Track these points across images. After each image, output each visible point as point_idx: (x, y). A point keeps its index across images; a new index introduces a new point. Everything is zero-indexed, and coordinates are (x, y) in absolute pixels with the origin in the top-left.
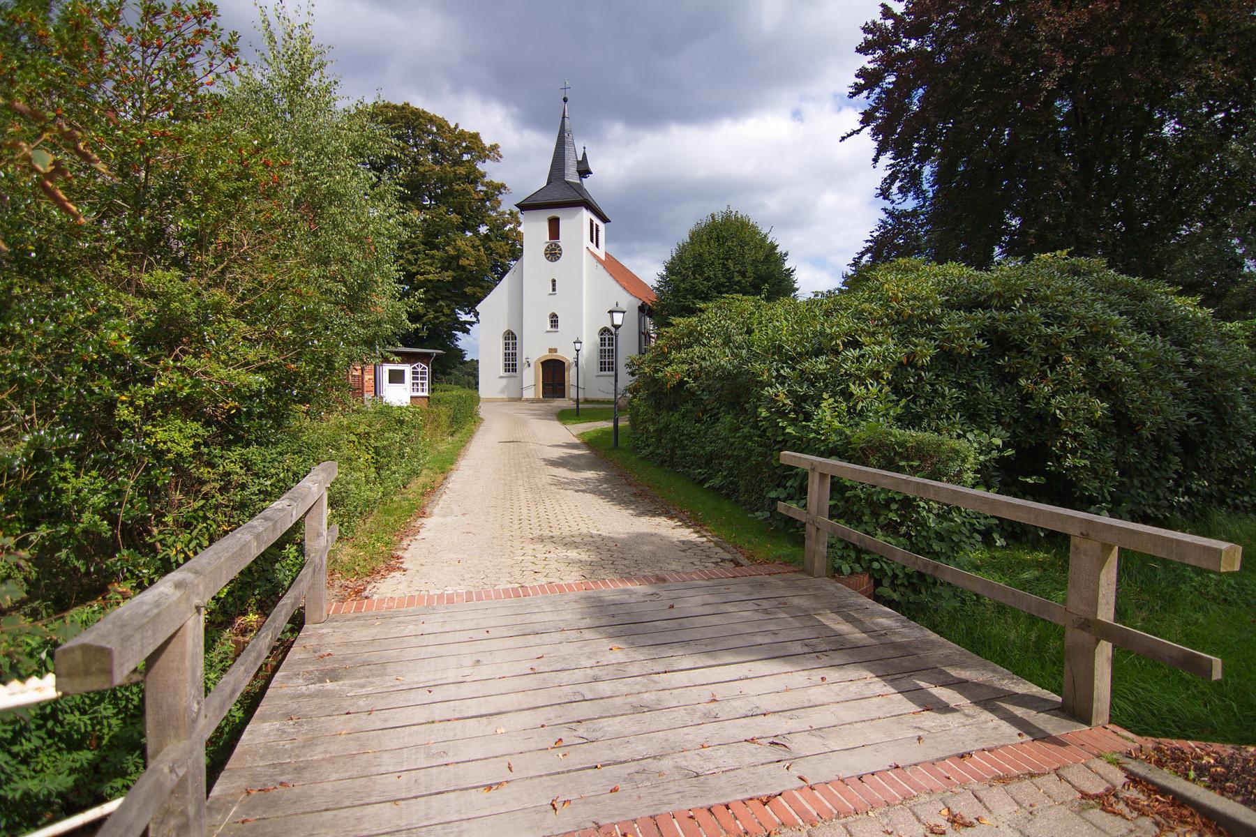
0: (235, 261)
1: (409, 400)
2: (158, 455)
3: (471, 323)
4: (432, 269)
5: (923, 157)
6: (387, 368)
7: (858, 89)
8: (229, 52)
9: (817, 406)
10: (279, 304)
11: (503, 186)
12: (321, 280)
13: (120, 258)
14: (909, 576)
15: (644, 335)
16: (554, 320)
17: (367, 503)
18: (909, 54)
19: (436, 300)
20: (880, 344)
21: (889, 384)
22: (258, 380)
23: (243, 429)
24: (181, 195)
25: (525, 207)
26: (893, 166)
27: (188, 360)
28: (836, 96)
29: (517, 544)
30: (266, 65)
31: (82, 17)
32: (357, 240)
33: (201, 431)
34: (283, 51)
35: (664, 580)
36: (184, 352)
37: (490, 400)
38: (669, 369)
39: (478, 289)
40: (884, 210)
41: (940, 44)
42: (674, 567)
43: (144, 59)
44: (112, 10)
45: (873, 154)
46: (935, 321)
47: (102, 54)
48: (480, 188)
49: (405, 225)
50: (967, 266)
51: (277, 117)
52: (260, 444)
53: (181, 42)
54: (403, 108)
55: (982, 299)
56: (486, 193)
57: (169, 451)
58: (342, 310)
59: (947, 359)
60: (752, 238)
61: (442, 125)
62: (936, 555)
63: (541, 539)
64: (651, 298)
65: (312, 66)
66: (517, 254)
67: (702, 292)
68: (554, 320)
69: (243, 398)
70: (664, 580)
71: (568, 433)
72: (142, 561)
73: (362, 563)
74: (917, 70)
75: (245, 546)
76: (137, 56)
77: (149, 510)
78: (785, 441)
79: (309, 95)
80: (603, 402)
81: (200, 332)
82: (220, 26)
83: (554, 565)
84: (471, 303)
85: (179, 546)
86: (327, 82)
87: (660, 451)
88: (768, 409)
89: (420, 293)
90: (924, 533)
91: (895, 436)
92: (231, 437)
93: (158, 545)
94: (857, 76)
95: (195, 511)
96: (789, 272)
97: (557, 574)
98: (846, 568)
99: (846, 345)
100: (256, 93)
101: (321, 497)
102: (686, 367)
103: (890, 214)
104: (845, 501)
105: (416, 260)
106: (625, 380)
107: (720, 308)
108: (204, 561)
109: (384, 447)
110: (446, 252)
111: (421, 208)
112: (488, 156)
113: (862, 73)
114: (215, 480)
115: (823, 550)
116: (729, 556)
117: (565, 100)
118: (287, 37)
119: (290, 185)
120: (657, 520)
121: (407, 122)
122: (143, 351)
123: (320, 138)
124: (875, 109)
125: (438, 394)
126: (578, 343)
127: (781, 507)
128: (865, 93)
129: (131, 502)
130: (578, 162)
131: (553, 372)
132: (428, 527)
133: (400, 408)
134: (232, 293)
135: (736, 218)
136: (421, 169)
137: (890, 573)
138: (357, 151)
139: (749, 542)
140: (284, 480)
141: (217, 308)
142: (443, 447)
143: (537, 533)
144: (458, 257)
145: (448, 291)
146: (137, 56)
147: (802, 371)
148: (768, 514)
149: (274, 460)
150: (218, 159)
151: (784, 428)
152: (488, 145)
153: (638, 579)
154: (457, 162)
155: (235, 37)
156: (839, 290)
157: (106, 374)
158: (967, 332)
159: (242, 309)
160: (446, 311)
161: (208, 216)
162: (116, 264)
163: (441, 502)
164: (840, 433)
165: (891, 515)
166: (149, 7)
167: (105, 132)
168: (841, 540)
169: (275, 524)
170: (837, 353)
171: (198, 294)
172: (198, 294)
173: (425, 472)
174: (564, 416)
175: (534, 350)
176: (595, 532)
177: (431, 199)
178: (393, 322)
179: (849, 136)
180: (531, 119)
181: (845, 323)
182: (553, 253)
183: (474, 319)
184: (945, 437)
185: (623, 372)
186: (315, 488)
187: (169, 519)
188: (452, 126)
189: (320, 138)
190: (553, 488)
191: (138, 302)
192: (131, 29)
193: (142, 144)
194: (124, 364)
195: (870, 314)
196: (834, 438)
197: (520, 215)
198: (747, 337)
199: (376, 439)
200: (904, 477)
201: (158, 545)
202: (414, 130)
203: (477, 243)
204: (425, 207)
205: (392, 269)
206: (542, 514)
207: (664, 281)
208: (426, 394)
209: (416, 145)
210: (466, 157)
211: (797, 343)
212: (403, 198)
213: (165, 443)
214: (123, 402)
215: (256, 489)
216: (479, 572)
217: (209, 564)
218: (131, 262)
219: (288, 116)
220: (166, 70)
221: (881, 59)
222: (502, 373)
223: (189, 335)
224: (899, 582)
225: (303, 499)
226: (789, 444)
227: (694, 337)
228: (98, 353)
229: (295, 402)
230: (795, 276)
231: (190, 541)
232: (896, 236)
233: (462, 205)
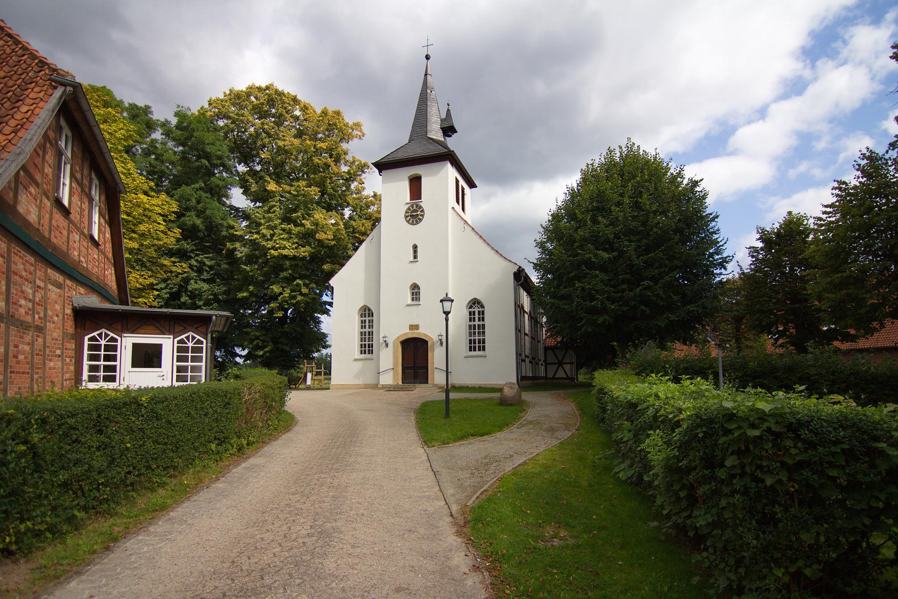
4: (287, 244)
6: (127, 343)
16: (415, 290)
54: (267, 88)
66: (376, 221)
68: (415, 290)
105: (272, 235)
117: (428, 57)
131: (415, 353)
152: (351, 124)
160: (305, 290)
182: (414, 215)
222: (358, 355)
230: (720, 224)
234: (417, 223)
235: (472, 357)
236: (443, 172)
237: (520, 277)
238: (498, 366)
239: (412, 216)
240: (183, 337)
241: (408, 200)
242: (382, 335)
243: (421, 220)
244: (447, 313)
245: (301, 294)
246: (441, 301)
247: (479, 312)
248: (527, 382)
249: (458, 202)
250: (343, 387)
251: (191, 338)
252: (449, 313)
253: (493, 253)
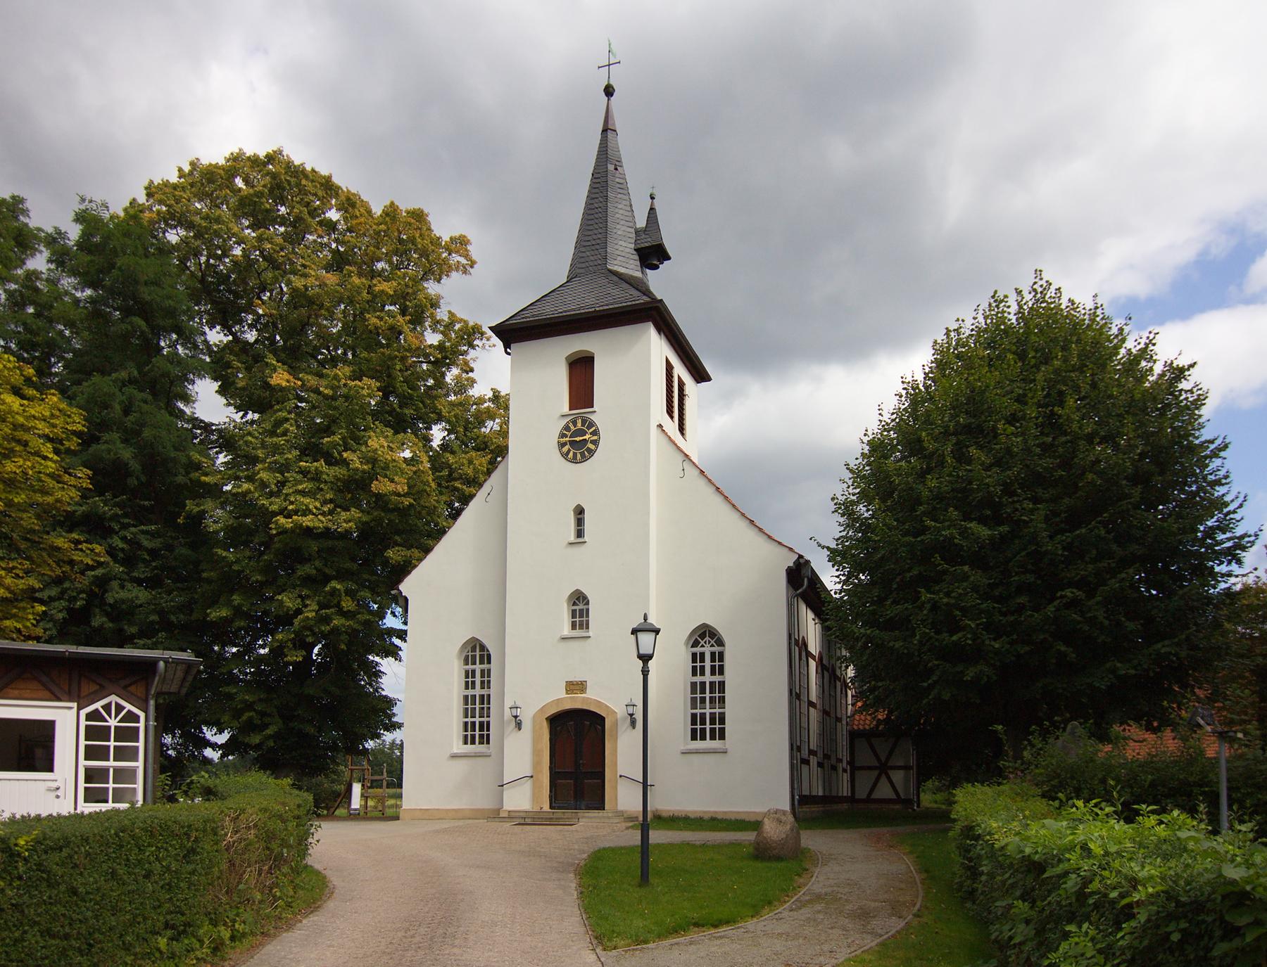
4: (312, 504)
16: (579, 603)
66: (497, 451)
68: (579, 603)
131: (577, 744)
144: (372, 476)
152: (446, 238)
160: (348, 604)
182: (578, 443)
222: (458, 747)
230: (1230, 463)
234: (584, 459)
235: (697, 752)
237: (800, 579)
238: (751, 774)
239: (572, 443)
240: (98, 705)
242: (508, 703)
244: (645, 658)
246: (634, 632)
247: (713, 654)
248: (813, 808)
250: (427, 815)
251: (115, 707)
252: (650, 657)
253: (742, 525)
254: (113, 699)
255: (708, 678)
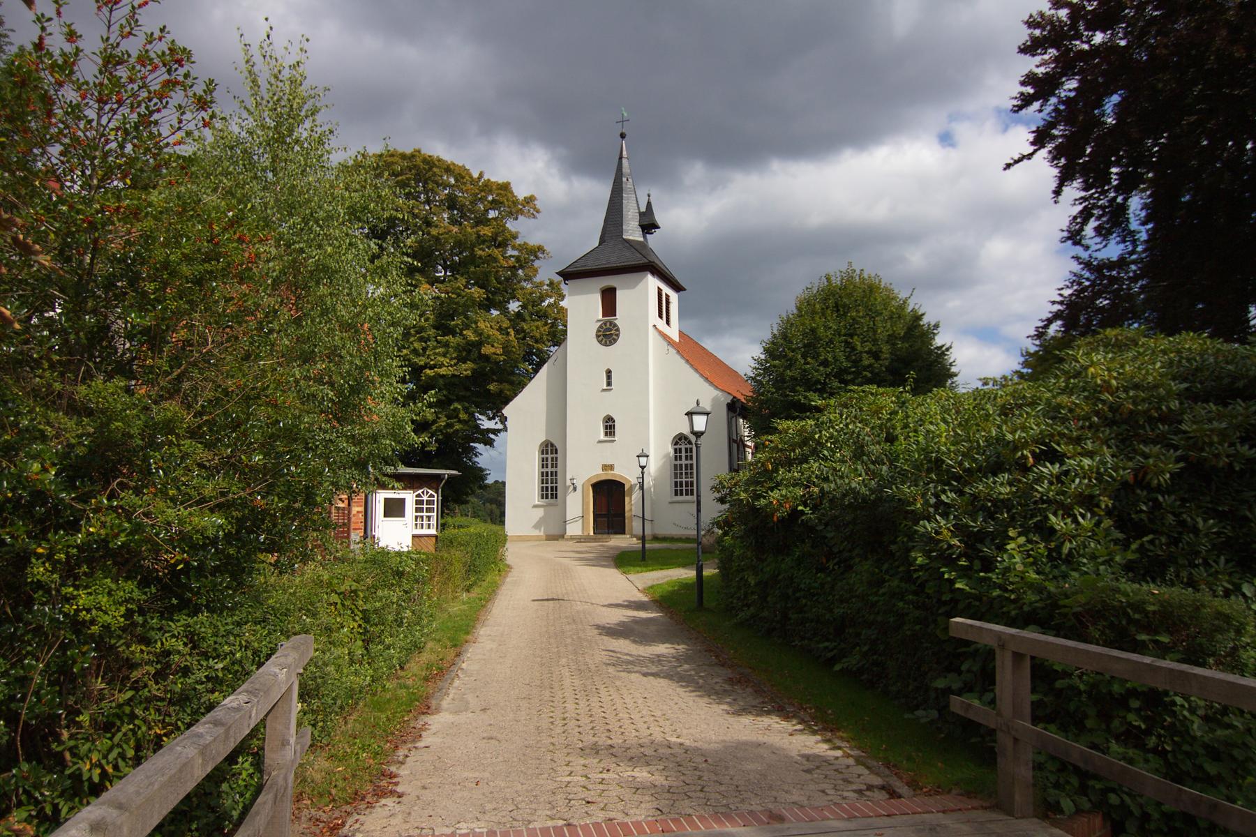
0: (194, 364)
1: (409, 542)
2: (77, 625)
3: (496, 432)
4: (446, 361)
5: (1128, 185)
6: (381, 496)
7: (1026, 101)
8: (203, 103)
9: (1001, 548)
10: (248, 420)
11: (541, 249)
12: (302, 382)
13: (52, 366)
14: (1168, 817)
15: (736, 444)
16: (610, 425)
17: (351, 693)
18: (1096, 51)
19: (450, 402)
20: (1090, 454)
21: (1109, 513)
22: (214, 522)
23: (191, 590)
24: (134, 281)
25: (568, 275)
26: (1084, 199)
27: (128, 497)
28: (998, 111)
29: (560, 756)
30: (245, 115)
31: (30, 72)
32: (350, 327)
33: (136, 594)
34: (267, 97)
35: (781, 819)
36: (123, 486)
37: (521, 539)
38: (775, 494)
39: (507, 386)
40: (1076, 258)
41: (1137, 38)
42: (795, 798)
43: (100, 117)
44: (65, 62)
45: (1053, 185)
46: (1172, 419)
47: (50, 114)
48: (510, 252)
49: (413, 306)
50: (1211, 336)
51: (256, 177)
52: (212, 611)
53: (146, 94)
54: (413, 156)
55: (1241, 384)
56: (518, 259)
57: (93, 622)
58: (328, 421)
59: (1197, 477)
60: (886, 305)
61: (461, 175)
62: (1209, 782)
63: (596, 750)
64: (744, 393)
65: (303, 114)
66: (558, 337)
67: (818, 382)
68: (610, 425)
69: (194, 547)
70: (781, 819)
71: (629, 586)
72: (46, 780)
73: (341, 784)
74: (1102, 71)
75: (187, 765)
76: (91, 114)
77: (60, 705)
78: (954, 601)
79: (297, 148)
80: (679, 540)
81: (146, 459)
82: (193, 74)
83: (615, 791)
84: (497, 404)
85: (95, 757)
86: (319, 130)
87: (765, 614)
88: (927, 554)
89: (431, 396)
90: (1186, 748)
91: (1126, 594)
92: (175, 601)
93: (68, 755)
94: (1023, 84)
95: (120, 706)
96: (942, 352)
97: (620, 806)
98: (1067, 804)
99: (1039, 458)
100: (232, 148)
101: (290, 689)
102: (800, 492)
103: (1087, 265)
104: (1055, 696)
105: (424, 349)
106: (713, 510)
107: (845, 406)
108: (131, 789)
109: (376, 611)
110: (465, 337)
111: (433, 281)
112: (521, 212)
113: (1030, 79)
114: (149, 663)
115: (1025, 772)
116: (877, 781)
117: (623, 136)
118: (273, 81)
119: (268, 261)
120: (766, 721)
121: (418, 173)
122: (70, 485)
123: (309, 201)
124: (1051, 125)
125: (451, 532)
126: (644, 456)
127: (956, 703)
128: (1036, 105)
129: (37, 693)
130: (641, 214)
131: (609, 498)
132: (433, 728)
133: (399, 554)
134: (189, 407)
135: (862, 280)
136: (434, 232)
137: (1137, 812)
138: (355, 214)
139: (909, 759)
140: (240, 662)
141: (168, 427)
142: (455, 608)
143: (589, 739)
144: (480, 344)
145: (467, 389)
146: (91, 114)
147: (975, 497)
148: (934, 714)
149: (229, 633)
150: (181, 236)
151: (952, 582)
153: (741, 816)
154: (482, 220)
155: (211, 85)
156: (1021, 376)
157: (20, 517)
158: (1223, 434)
159: (200, 427)
160: (463, 416)
161: (165, 309)
162: (47, 374)
163: (452, 691)
164: (1039, 589)
165: (1131, 717)
166: (111, 55)
167: (47, 209)
168: (1053, 758)
169: (227, 732)
170: (1025, 469)
171: (146, 408)
172: (146, 408)
173: (430, 645)
174: (623, 560)
175: (582, 468)
176: (674, 739)
177: (445, 268)
178: (394, 435)
179: (1016, 162)
180: (579, 163)
181: (1034, 425)
182: (608, 335)
183: (500, 426)
184: (1205, 596)
185: (708, 498)
186: (282, 674)
187: (84, 718)
188: (476, 175)
189: (309, 201)
190: (611, 670)
191: (70, 423)
192: (87, 83)
193: (90, 223)
194: (43, 504)
195: (1071, 411)
196: (1031, 597)
197: (563, 286)
198: (887, 446)
199: (366, 599)
200: (1147, 660)
201: (68, 755)
202: (425, 183)
203: (506, 324)
204: (437, 280)
205: (394, 365)
206: (596, 711)
207: (764, 368)
208: (433, 531)
209: (428, 202)
210: (492, 214)
211: (964, 455)
212: (411, 271)
213: (89, 611)
214: (39, 556)
215: (202, 675)
216: (505, 800)
217: (138, 793)
218: (64, 368)
219: (270, 175)
220: (126, 130)
221: (1056, 60)
222: (536, 500)
223: (130, 463)
224: (1153, 826)
225: (267, 692)
226: (961, 606)
227: (809, 448)
228: (13, 490)
229: (262, 551)
231: (110, 750)
232: (1098, 295)
233: (486, 275)
234: (611, 344)
236: (641, 285)
241: (600, 317)
242: (568, 477)
243: (615, 341)
244: (643, 468)
245: (460, 421)
249: (660, 316)
251: (428, 494)
254: (425, 489)
255: (549, 469)
